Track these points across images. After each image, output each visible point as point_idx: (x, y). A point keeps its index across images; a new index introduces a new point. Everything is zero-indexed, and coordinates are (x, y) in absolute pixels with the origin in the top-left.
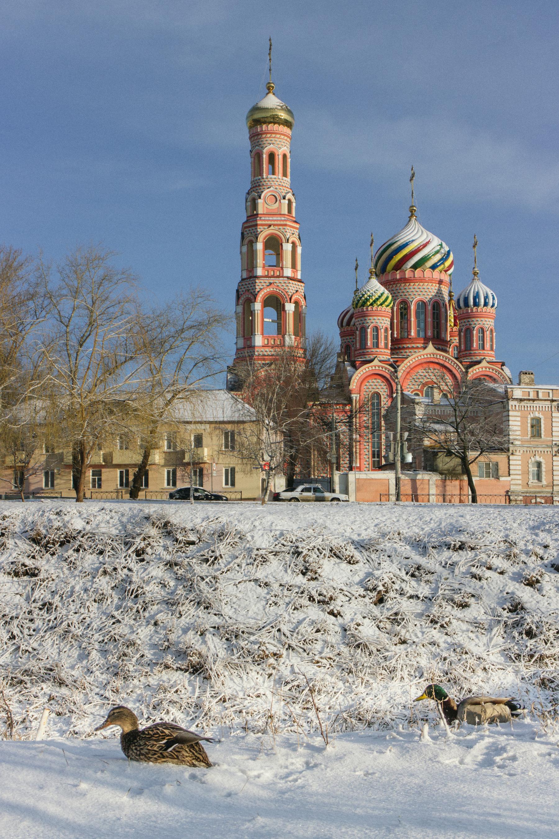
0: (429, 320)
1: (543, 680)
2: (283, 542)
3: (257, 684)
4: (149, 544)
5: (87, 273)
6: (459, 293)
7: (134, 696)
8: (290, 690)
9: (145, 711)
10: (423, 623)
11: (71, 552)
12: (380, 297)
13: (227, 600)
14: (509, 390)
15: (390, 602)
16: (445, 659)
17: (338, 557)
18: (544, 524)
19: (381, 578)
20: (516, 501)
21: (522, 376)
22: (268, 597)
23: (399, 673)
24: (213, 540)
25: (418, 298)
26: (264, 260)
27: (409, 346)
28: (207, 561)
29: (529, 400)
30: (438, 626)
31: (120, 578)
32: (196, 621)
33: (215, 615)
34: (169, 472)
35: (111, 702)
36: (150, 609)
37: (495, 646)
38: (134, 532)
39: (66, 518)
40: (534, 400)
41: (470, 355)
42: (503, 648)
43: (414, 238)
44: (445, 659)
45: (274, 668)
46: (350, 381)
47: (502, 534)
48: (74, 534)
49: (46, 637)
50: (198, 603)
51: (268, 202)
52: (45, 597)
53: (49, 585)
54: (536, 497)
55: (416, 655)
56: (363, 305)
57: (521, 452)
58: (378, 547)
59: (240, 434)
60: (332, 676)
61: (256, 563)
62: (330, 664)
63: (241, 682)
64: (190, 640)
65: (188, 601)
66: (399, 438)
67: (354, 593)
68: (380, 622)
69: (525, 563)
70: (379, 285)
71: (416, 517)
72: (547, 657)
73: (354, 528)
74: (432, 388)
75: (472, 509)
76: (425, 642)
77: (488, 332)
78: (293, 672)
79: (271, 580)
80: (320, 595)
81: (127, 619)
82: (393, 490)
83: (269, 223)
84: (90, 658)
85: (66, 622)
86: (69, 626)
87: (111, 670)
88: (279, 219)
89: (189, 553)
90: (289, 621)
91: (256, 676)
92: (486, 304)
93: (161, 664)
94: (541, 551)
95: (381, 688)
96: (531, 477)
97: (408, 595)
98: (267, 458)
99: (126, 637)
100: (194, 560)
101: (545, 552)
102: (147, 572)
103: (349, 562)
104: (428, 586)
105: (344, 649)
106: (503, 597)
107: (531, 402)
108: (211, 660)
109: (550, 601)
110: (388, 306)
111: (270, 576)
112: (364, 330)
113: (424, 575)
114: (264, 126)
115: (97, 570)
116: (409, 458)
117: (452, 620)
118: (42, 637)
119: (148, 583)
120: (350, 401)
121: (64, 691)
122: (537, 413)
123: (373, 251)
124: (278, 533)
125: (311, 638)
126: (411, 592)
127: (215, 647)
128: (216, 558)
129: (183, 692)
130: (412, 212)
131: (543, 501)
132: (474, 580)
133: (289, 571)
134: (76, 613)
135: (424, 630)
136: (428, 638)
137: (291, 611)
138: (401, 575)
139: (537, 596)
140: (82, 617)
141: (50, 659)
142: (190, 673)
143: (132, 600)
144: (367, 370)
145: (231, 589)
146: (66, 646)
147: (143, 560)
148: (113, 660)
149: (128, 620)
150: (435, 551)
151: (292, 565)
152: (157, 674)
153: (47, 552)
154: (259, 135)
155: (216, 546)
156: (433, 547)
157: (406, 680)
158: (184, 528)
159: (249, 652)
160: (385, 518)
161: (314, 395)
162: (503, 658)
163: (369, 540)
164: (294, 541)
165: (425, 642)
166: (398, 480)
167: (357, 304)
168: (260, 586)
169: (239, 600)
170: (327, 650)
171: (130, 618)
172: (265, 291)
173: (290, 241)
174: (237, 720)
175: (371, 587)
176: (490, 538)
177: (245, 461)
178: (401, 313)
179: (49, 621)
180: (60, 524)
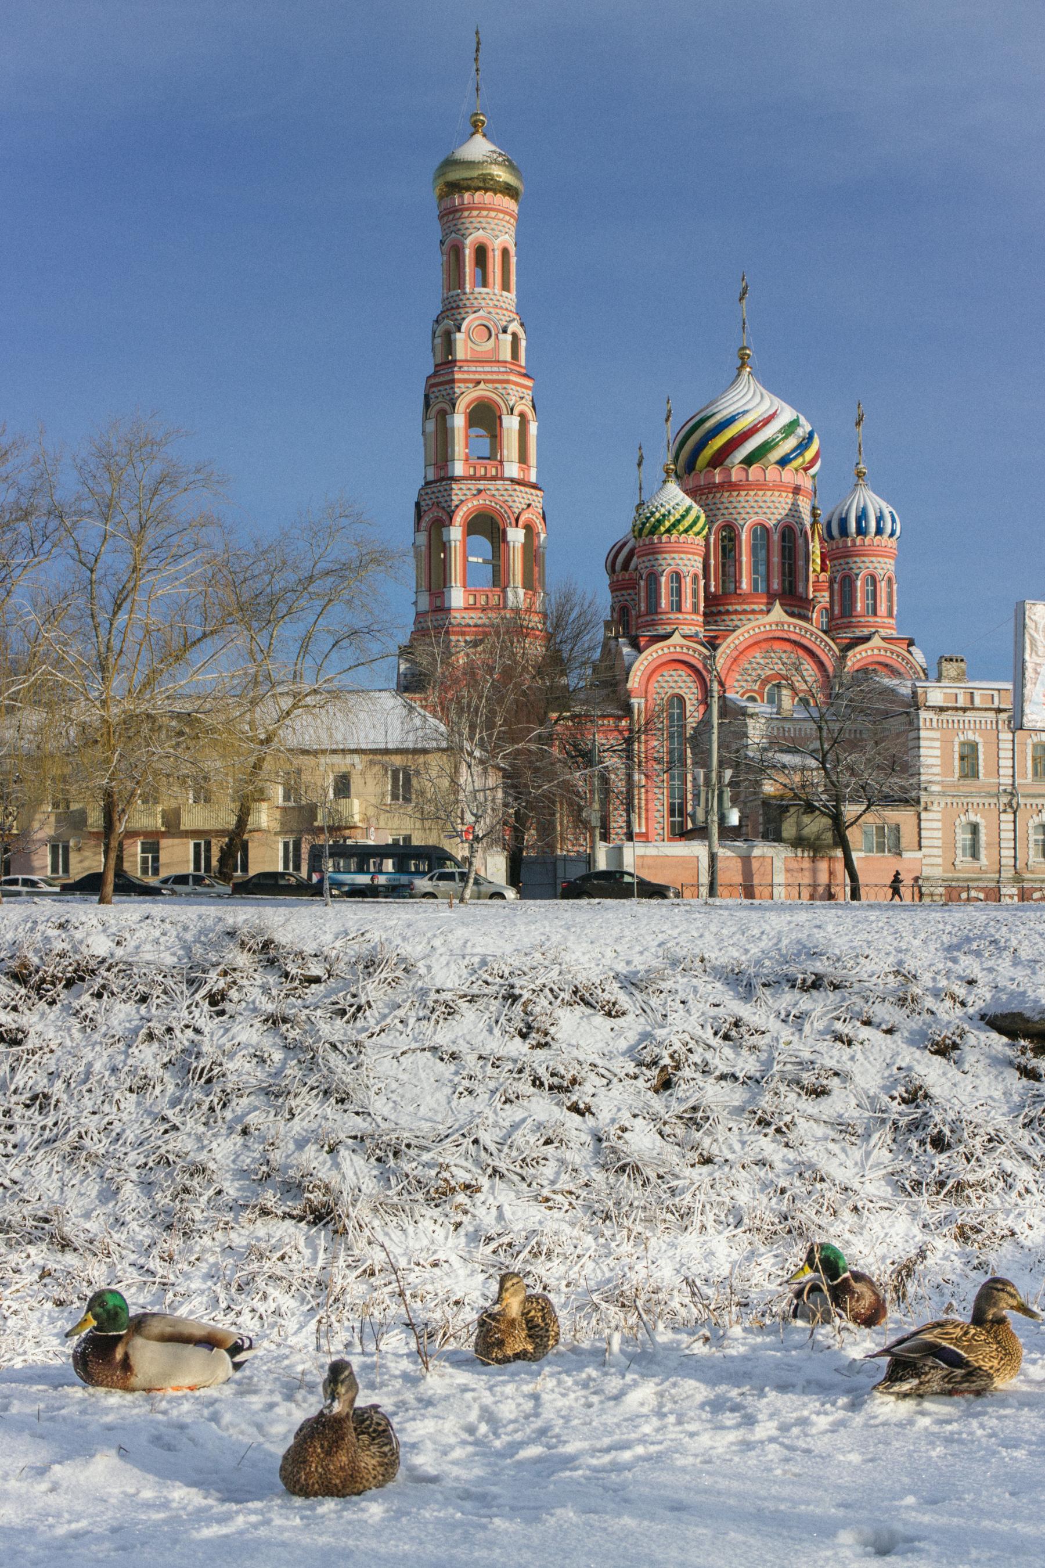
0: (776, 559)
1: (961, 1228)
2: (485, 976)
3: (433, 1242)
4: (234, 983)
5: (130, 470)
6: (830, 510)
7: (204, 1267)
8: (494, 1252)
9: (222, 1296)
10: (743, 1125)
11: (86, 998)
12: (683, 517)
13: (380, 1085)
14: (920, 690)
15: (684, 1087)
16: (783, 1191)
17: (588, 1004)
18: (968, 940)
19: (667, 1042)
20: (932, 895)
21: (944, 664)
22: (457, 1079)
23: (697, 1219)
24: (355, 974)
25: (755, 518)
26: (467, 447)
27: (738, 608)
28: (343, 1013)
29: (956, 709)
30: (771, 1130)
31: (179, 1048)
32: (320, 1126)
33: (357, 1113)
34: (286, 845)
35: (158, 1280)
36: (234, 1104)
37: (877, 1165)
38: (206, 960)
39: (78, 935)
40: (964, 710)
41: (849, 626)
42: (890, 1169)
43: (746, 408)
44: (783, 1191)
45: (466, 1212)
46: (628, 674)
47: (891, 960)
48: (93, 964)
49: (38, 1159)
50: (326, 1092)
51: (474, 337)
52: (36, 1083)
53: (44, 1061)
54: (968, 888)
55: (730, 1184)
56: (652, 532)
57: (942, 805)
58: (665, 985)
59: (418, 773)
60: (573, 1225)
61: (434, 1017)
62: (570, 1204)
63: (403, 1238)
64: (309, 1161)
65: (305, 1089)
66: (714, 780)
67: (617, 1071)
68: (665, 1123)
69: (933, 1013)
70: (682, 494)
71: (734, 929)
72: (971, 1186)
73: (619, 949)
74: (778, 686)
75: (840, 912)
76: (747, 1160)
77: (883, 583)
78: (500, 1217)
79: (462, 1047)
80: (553, 1075)
81: (190, 1123)
82: (704, 879)
83: (477, 377)
84: (120, 1196)
85: (76, 1130)
86: (81, 1137)
87: (159, 1219)
88: (495, 369)
89: (310, 999)
90: (496, 1125)
91: (433, 1227)
92: (879, 531)
93: (255, 1207)
94: (961, 991)
95: (664, 1247)
96: (959, 852)
97: (717, 1073)
98: (469, 818)
99: (189, 1158)
100: (319, 1012)
101: (969, 993)
102: (230, 1034)
103: (609, 1014)
104: (754, 1057)
105: (598, 1176)
106: (891, 1076)
107: (960, 713)
108: (347, 1198)
109: (977, 1082)
110: (698, 533)
111: (461, 1041)
112: (653, 578)
113: (747, 1037)
114: (467, 196)
115: (136, 1031)
116: (734, 818)
117: (796, 1120)
118: (30, 1159)
119: (231, 1055)
120: (627, 709)
121: (70, 1259)
122: (970, 733)
123: (671, 431)
124: (476, 960)
125: (534, 1155)
126: (724, 1069)
127: (356, 1174)
128: (359, 1008)
129: (295, 1258)
130: (742, 358)
131: (982, 896)
132: (839, 1044)
133: (497, 1031)
134: (94, 1113)
135: (746, 1138)
136: (751, 1153)
137: (500, 1105)
138: (704, 1036)
139: (953, 1072)
140: (105, 1121)
141: (43, 1199)
142: (308, 1222)
143: (202, 1087)
144: (660, 652)
145: (387, 1066)
146: (75, 1175)
147: (221, 1013)
148: (163, 1199)
149: (192, 1125)
150: (767, 992)
151: (502, 1020)
152: (246, 1225)
153: (40, 999)
154: (457, 211)
155: (361, 984)
156: (764, 985)
157: (711, 1231)
158: (301, 953)
159: (419, 1182)
160: (677, 931)
161: (561, 699)
162: (889, 1189)
163: (647, 971)
164: (506, 975)
165: (747, 1160)
166: (713, 857)
167: (641, 530)
168: (442, 1059)
169: (403, 1085)
170: (564, 1177)
171: (196, 1121)
172: (470, 505)
173: (516, 411)
174: (395, 1309)
175: (649, 1059)
176: (868, 967)
177: (427, 824)
178: (724, 548)
179: (43, 1128)
180: (67, 946)
